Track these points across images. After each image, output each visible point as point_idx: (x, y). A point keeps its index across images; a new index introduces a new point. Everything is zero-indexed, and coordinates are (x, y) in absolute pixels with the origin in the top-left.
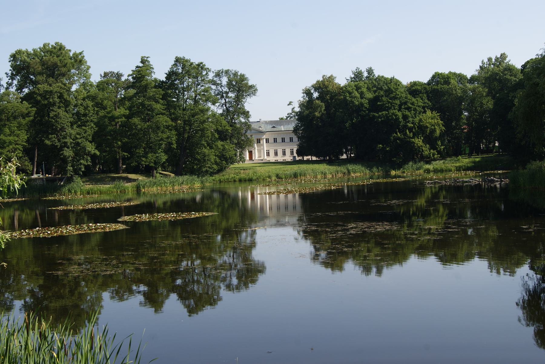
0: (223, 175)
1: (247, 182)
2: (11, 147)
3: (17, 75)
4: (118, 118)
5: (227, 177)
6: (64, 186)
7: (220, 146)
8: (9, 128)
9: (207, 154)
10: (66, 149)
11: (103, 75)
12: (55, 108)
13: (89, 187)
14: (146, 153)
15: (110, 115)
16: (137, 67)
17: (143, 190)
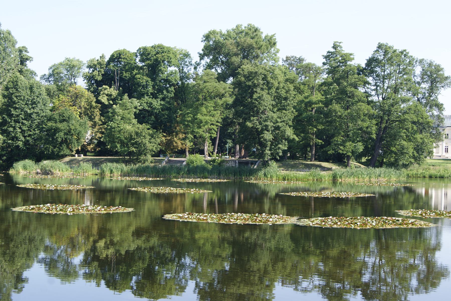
0: (411, 170)
1: (438, 179)
2: (206, 127)
3: (208, 55)
4: (315, 103)
5: (415, 172)
6: (259, 169)
7: (419, 140)
8: (206, 108)
9: (406, 146)
10: (266, 132)
11: (285, 59)
12: (258, 90)
13: (283, 172)
14: (344, 142)
15: (307, 100)
16: (329, 52)
17: (340, 180)
